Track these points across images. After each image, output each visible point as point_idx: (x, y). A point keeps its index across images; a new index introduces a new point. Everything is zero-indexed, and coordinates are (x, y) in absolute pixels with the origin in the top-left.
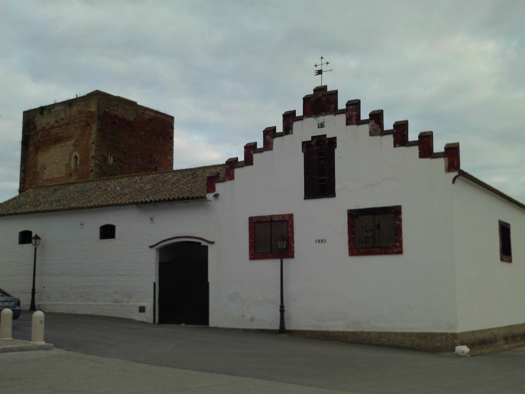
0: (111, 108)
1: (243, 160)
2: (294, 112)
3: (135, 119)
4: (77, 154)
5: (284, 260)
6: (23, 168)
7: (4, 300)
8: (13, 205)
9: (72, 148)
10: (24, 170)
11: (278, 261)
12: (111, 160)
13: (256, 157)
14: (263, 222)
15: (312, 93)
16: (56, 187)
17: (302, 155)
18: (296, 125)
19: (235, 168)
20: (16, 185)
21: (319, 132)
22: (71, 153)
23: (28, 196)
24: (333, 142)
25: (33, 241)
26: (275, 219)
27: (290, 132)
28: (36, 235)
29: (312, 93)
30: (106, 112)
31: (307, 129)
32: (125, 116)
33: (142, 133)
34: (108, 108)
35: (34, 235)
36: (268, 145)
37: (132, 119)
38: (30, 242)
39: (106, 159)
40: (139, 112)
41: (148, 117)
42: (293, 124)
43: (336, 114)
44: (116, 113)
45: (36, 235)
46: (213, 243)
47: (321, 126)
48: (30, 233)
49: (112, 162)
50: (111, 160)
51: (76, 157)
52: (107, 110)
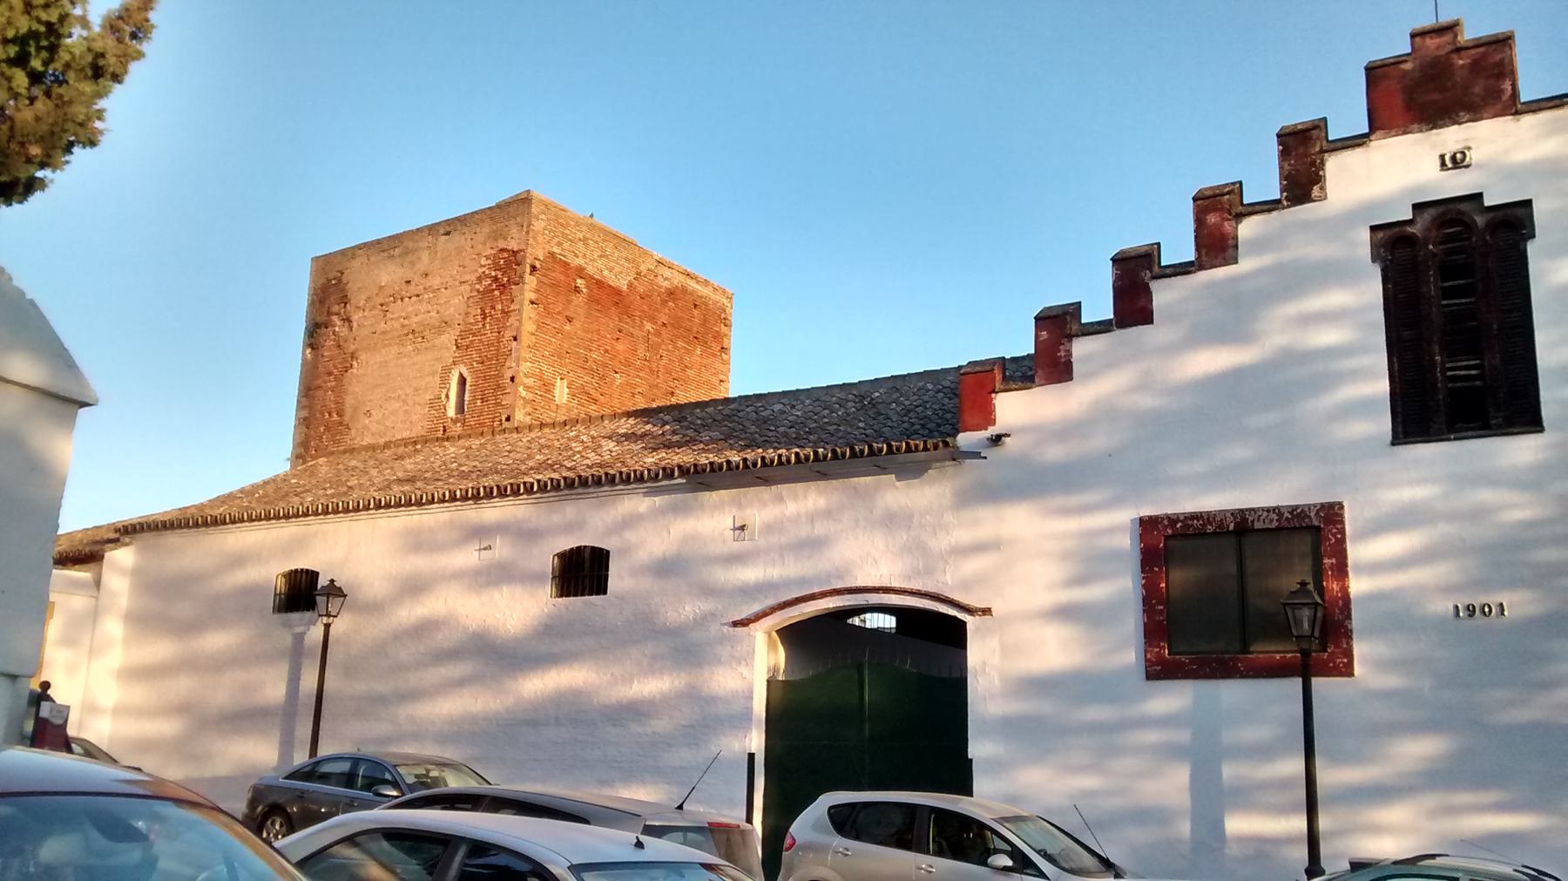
0: (566, 245)
1: (1030, 349)
2: (1321, 125)
3: (630, 285)
4: (466, 374)
5: (1316, 682)
6: (305, 413)
7: (1439, 861)
8: (265, 496)
9: (450, 353)
10: (305, 419)
11: (1296, 684)
12: (561, 393)
13: (1163, 295)
14: (1202, 534)
15: (1404, 47)
16: (401, 450)
17: (1376, 272)
18: (1336, 168)
19: (1070, 337)
20: (287, 448)
21: (1456, 185)
22: (446, 372)
23: (312, 474)
24: (1514, 222)
25: (320, 600)
26: (1257, 526)
27: (1316, 191)
28: (332, 581)
29: (1404, 47)
30: (552, 254)
31: (1395, 173)
32: (606, 273)
33: (649, 326)
34: (560, 244)
35: (322, 582)
36: (1215, 247)
37: (623, 284)
38: (310, 605)
39: (547, 387)
40: (643, 268)
41: (666, 284)
42: (1323, 163)
43: (1517, 113)
44: (580, 261)
45: (332, 581)
46: (986, 611)
47: (1457, 162)
48: (313, 576)
49: (565, 398)
50: (561, 393)
51: (462, 381)
52: (556, 250)
